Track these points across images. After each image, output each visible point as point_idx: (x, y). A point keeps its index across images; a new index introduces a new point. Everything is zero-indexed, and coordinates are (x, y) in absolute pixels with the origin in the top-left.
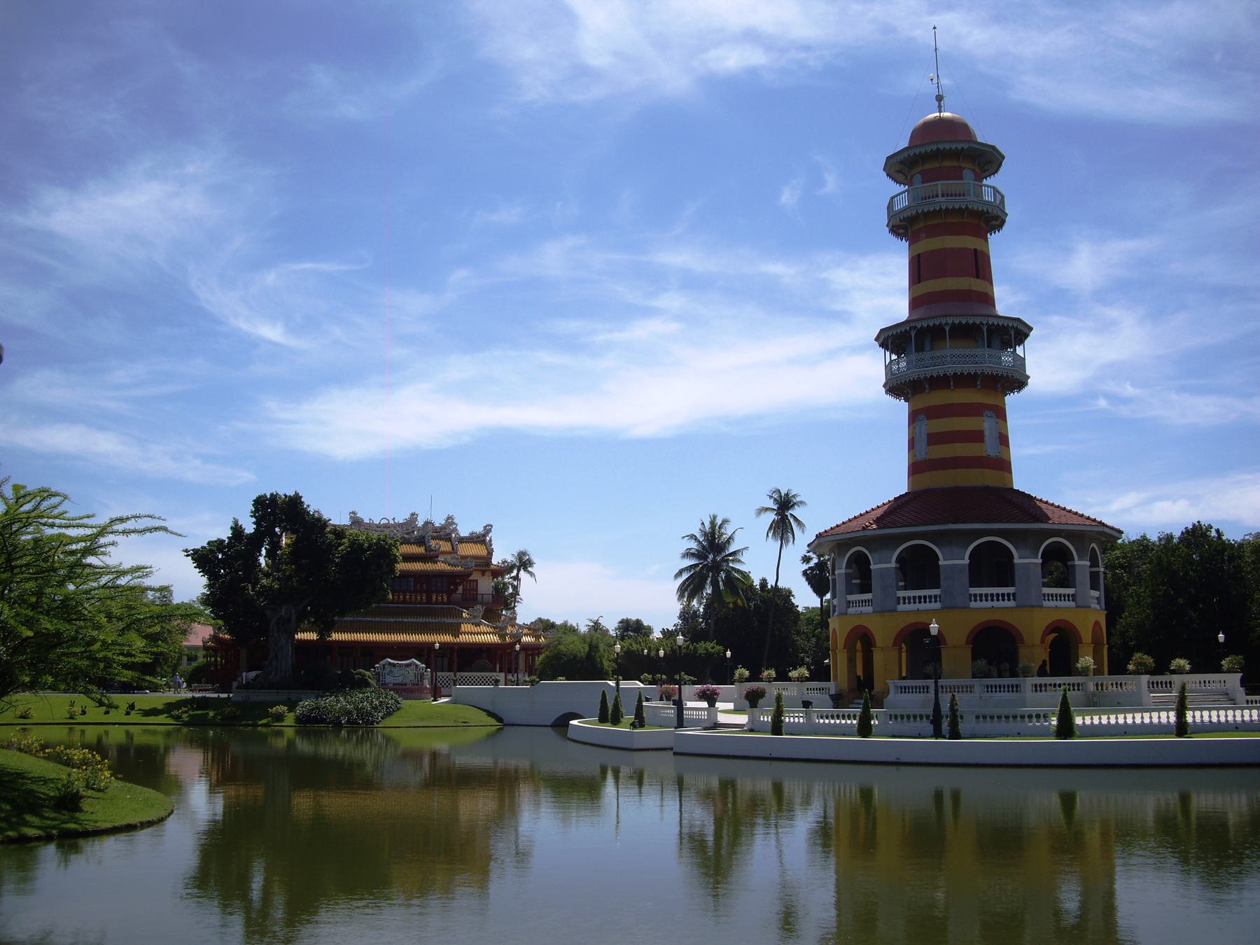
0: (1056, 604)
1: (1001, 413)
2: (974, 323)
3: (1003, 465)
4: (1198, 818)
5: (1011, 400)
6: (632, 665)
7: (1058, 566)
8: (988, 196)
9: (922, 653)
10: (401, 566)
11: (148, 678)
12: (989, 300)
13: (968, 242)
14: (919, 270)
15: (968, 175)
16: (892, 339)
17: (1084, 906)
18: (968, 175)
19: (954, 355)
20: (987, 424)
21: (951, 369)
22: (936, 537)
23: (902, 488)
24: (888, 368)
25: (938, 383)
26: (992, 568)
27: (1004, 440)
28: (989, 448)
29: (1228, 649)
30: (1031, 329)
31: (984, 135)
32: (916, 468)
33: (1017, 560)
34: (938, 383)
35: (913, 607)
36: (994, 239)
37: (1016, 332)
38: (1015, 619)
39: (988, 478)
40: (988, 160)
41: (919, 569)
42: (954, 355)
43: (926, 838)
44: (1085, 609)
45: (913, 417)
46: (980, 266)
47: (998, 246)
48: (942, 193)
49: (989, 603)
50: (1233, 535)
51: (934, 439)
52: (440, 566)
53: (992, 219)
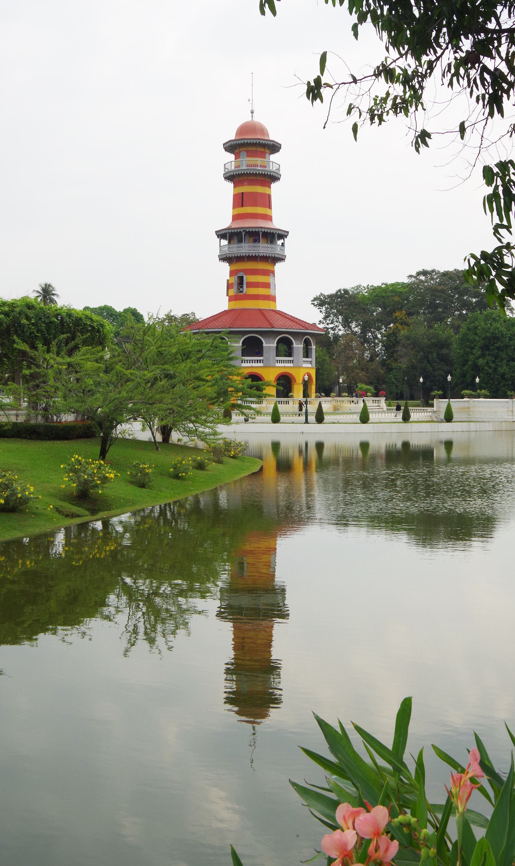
2: (255, 231)
5: (278, 267)
12: (269, 218)
14: (240, 200)
19: (252, 246)
30: (288, 232)
35: (249, 365)
42: (252, 246)
46: (266, 201)
48: (247, 163)
53: (273, 178)
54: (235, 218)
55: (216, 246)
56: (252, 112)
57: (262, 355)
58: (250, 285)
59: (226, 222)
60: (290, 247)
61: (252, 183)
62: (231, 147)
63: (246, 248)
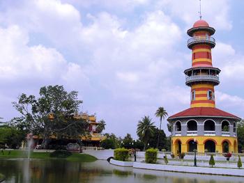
12: (211, 64)
14: (194, 56)
16: (189, 73)
19: (202, 77)
26: (210, 126)
38: (230, 139)
40: (211, 32)
41: (192, 126)
42: (202, 77)
44: (231, 136)
46: (209, 56)
53: (212, 45)
54: (193, 64)
55: (184, 78)
57: (196, 130)
58: (205, 95)
59: (189, 66)
60: (221, 77)
61: (198, 48)
62: (191, 33)
63: (193, 78)
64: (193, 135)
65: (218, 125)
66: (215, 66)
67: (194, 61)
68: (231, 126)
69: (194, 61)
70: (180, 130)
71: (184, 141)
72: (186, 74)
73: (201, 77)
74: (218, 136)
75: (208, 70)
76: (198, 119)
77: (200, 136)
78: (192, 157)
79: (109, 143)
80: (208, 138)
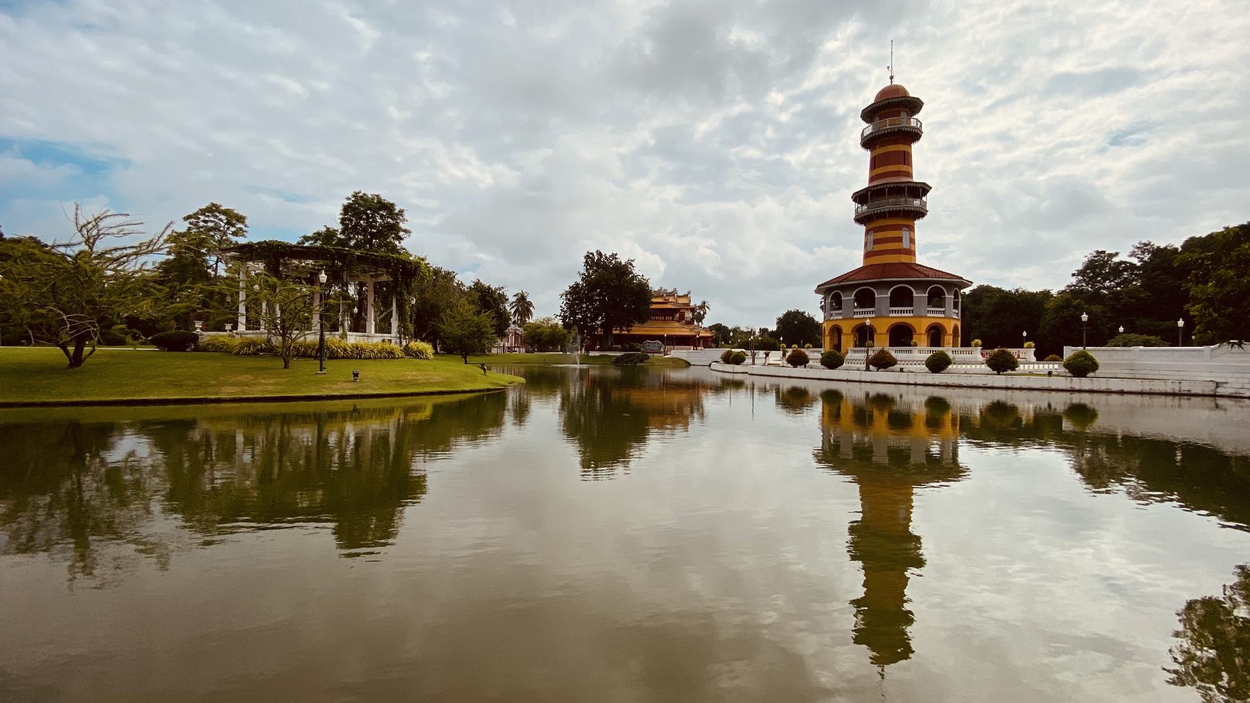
0: (934, 316)
1: (911, 229)
3: (911, 253)
4: (374, 436)
6: (746, 345)
7: (936, 298)
8: (913, 123)
9: (864, 335)
10: (654, 306)
11: (619, 354)
12: (909, 175)
13: (901, 148)
14: (874, 164)
15: (904, 115)
16: (860, 197)
17: (942, 453)
18: (904, 115)
19: (891, 201)
20: (905, 235)
21: (887, 208)
22: (874, 285)
23: (860, 264)
24: (857, 210)
25: (882, 216)
26: (901, 298)
27: (912, 241)
28: (905, 244)
29: (1028, 339)
31: (912, 93)
32: (867, 255)
33: (915, 294)
34: (882, 216)
36: (915, 146)
37: (923, 190)
39: (904, 259)
40: (914, 106)
41: (865, 299)
42: (891, 201)
43: (862, 416)
44: (951, 319)
45: (867, 232)
46: (906, 158)
47: (915, 148)
48: (888, 124)
49: (901, 315)
50: (1228, 449)
51: (876, 242)
52: (669, 306)
53: (915, 135)
54: (872, 179)
56: (892, 78)
59: (863, 183)
62: (869, 114)
64: (867, 317)
65: (920, 296)
66: (917, 178)
67: (880, 170)
68: (949, 297)
69: (880, 170)
70: (840, 308)
71: (847, 327)
72: (855, 200)
73: (888, 204)
74: (921, 316)
75: (1055, 420)
76: (874, 285)
77: (883, 318)
78: (82, 564)
79: (721, 335)
80: (934, 321)
